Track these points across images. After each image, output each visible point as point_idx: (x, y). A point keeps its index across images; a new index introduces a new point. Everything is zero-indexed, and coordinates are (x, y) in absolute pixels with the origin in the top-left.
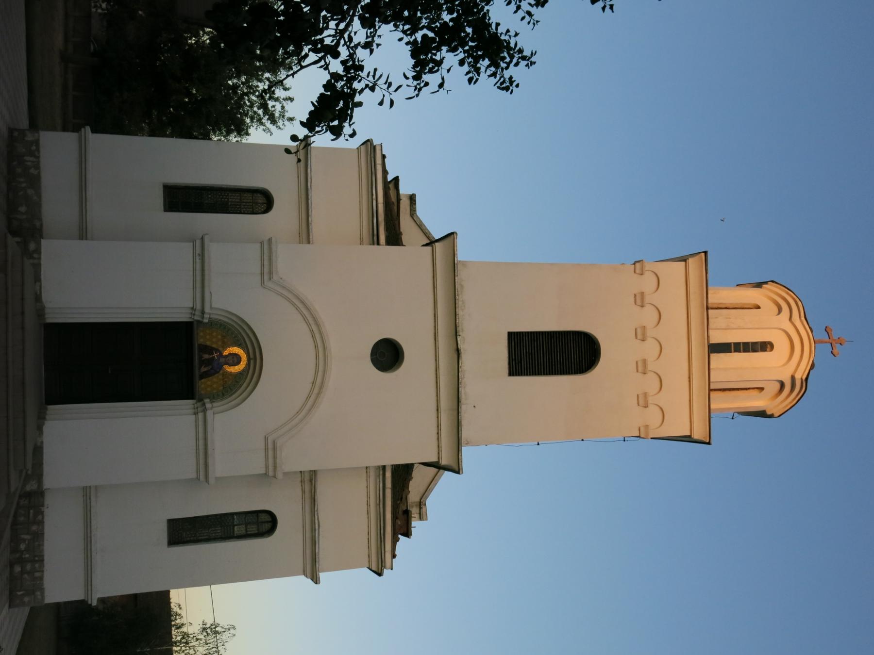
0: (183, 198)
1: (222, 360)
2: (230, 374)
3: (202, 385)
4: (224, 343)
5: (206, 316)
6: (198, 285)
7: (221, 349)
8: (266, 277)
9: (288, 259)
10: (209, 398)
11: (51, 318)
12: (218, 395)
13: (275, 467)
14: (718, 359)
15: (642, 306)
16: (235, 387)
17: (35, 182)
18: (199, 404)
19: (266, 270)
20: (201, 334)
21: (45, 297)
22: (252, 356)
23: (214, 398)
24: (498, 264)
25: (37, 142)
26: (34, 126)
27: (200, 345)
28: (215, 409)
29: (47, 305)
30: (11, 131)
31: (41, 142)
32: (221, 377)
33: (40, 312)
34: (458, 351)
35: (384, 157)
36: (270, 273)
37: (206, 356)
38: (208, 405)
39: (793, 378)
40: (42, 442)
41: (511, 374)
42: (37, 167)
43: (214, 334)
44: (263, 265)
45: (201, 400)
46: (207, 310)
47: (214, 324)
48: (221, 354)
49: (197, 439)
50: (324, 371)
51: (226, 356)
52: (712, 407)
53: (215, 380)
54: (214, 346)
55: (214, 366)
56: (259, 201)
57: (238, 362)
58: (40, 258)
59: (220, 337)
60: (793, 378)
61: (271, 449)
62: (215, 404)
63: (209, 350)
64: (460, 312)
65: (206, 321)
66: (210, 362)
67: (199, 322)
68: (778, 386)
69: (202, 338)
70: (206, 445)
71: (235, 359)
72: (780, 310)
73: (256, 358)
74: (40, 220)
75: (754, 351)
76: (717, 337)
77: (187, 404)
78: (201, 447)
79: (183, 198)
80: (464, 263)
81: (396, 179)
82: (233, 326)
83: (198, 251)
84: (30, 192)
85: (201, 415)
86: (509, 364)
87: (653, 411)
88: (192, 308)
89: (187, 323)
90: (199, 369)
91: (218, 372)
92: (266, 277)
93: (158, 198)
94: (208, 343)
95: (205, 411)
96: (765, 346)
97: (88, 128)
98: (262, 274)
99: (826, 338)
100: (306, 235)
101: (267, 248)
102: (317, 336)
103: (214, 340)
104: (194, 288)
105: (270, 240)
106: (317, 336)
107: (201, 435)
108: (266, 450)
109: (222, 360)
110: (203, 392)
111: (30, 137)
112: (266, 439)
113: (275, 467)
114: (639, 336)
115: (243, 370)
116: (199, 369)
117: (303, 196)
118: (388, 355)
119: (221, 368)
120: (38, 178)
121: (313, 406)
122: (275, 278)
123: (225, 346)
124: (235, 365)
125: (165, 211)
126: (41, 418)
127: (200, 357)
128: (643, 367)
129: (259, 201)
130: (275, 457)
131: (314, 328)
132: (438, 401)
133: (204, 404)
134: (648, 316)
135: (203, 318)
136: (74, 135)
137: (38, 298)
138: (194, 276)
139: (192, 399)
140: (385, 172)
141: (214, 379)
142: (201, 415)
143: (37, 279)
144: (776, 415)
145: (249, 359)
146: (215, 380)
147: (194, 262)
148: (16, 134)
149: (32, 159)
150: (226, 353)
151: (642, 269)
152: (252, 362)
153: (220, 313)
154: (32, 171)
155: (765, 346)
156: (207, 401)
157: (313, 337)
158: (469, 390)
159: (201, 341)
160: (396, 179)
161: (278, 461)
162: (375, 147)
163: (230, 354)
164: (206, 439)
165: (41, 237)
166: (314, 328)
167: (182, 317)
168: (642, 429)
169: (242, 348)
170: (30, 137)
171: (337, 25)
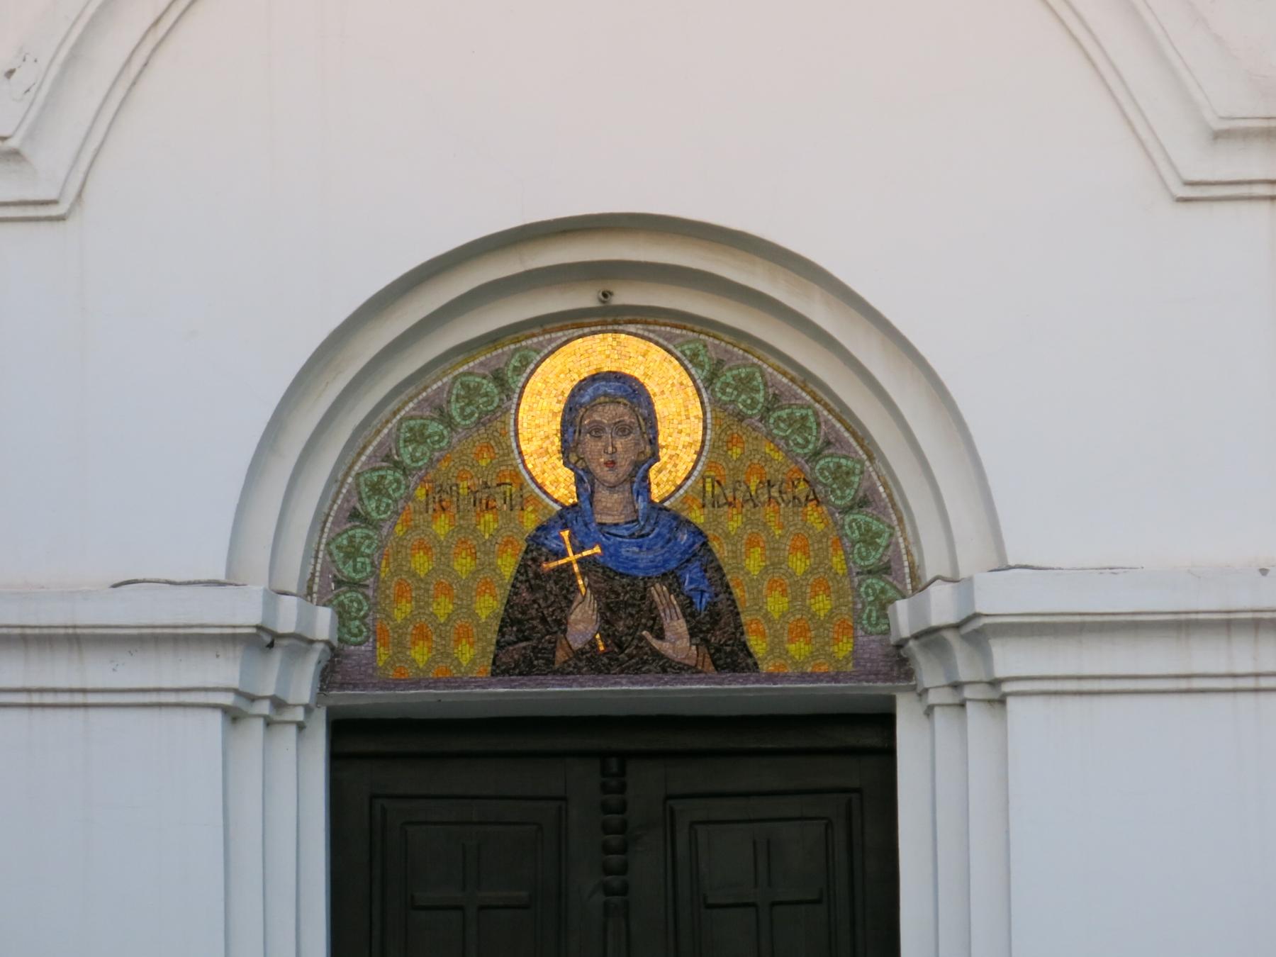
1: (612, 507)
2: (714, 448)
3: (793, 653)
4: (482, 501)
5: (288, 617)
6: (60, 671)
7: (530, 521)
10: (883, 606)
12: (377, 489)
18: (929, 673)
20: (420, 654)
22: (586, 298)
23: (888, 571)
27: (500, 669)
28: (970, 559)
32: (734, 523)
37: (583, 622)
38: (941, 606)
43: (421, 563)
46: (243, 610)
48: (567, 515)
49: (1187, 686)
51: (585, 479)
53: (754, 563)
54: (507, 566)
55: (656, 571)
57: (629, 391)
59: (441, 527)
62: (933, 564)
63: (528, 630)
65: (323, 623)
66: (626, 605)
69: (449, 656)
70: (1227, 625)
71: (606, 414)
77: (930, 762)
82: (354, 447)
85: (1009, 659)
88: (233, 716)
89: (337, 759)
90: (667, 666)
91: (701, 547)
94: (489, 607)
95: (976, 631)
103: (463, 565)
104: (80, 701)
109: (612, 507)
110: (844, 648)
112: (1197, 194)
115: (690, 361)
116: (667, 666)
119: (664, 518)
123: (511, 486)
124: (650, 423)
127: (589, 661)
133: (930, 636)
135: (302, 641)
139: (885, 721)
141: (747, 567)
142: (1009, 659)
145: (608, 318)
146: (754, 563)
150: (560, 484)
152: (626, 296)
156: (904, 618)
159: (471, 655)
163: (568, 450)
164: (1183, 626)
167: (293, 787)
169: (527, 366)
171: (414, 450)
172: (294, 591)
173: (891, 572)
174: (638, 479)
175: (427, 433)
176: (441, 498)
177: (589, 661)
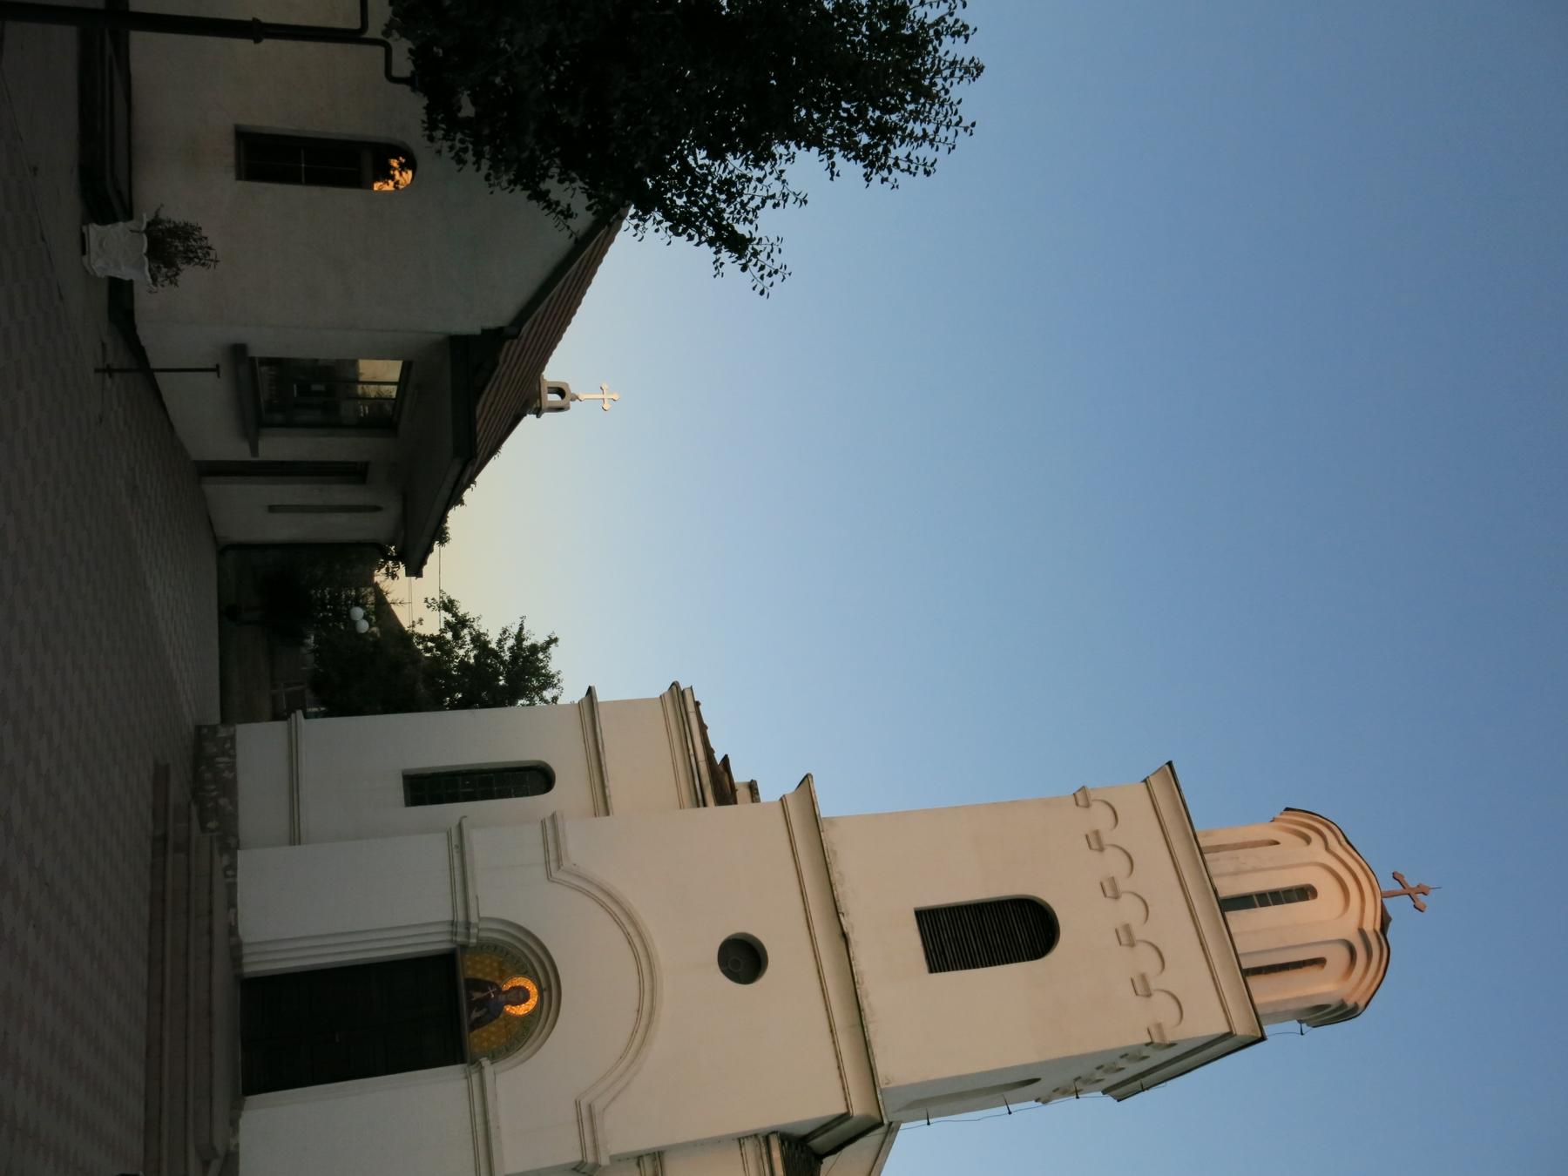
0: (427, 788)
1: (502, 998)
2: (517, 1018)
3: (475, 1039)
5: (474, 931)
6: (458, 887)
8: (553, 865)
9: (586, 843)
11: (256, 965)
13: (595, 1147)
14: (1240, 920)
15: (1149, 995)
16: (521, 1036)
17: (229, 788)
19: (552, 856)
21: (241, 931)
22: (544, 985)
24: (877, 816)
25: (232, 739)
26: (226, 719)
27: (467, 980)
29: (246, 939)
30: (199, 728)
31: (238, 738)
33: (236, 953)
34: (845, 936)
35: (697, 704)
36: (559, 859)
37: (477, 995)
39: (1362, 932)
40: (237, 1146)
41: (932, 969)
42: (232, 767)
44: (547, 851)
45: (475, 1062)
46: (474, 919)
47: (490, 948)
48: (499, 991)
50: (653, 989)
52: (1256, 1001)
55: (491, 1010)
56: (538, 778)
57: (526, 998)
58: (235, 876)
60: (1362, 932)
61: (587, 1119)
64: (839, 890)
67: (464, 947)
68: (1344, 953)
69: (470, 969)
70: (486, 1122)
72: (1308, 840)
73: (551, 989)
74: (236, 836)
75: (1289, 901)
76: (1228, 888)
77: (458, 1068)
78: (480, 1128)
79: (427, 788)
80: (831, 821)
81: (726, 759)
83: (455, 841)
84: (222, 801)
86: (927, 958)
87: (1161, 1001)
88: (453, 923)
90: (470, 1013)
91: (496, 1017)
92: (553, 865)
93: (398, 791)
94: (480, 976)
96: (1305, 893)
97: (300, 713)
98: (547, 863)
99: (1397, 887)
100: (603, 805)
101: (551, 829)
102: (636, 940)
104: (453, 893)
105: (553, 817)
106: (636, 940)
107: (478, 1109)
108: (579, 1121)
109: (502, 998)
111: (223, 733)
112: (577, 1104)
113: (595, 1147)
114: (1109, 893)
117: (594, 764)
118: (743, 958)
119: (501, 1010)
120: (234, 781)
121: (617, 902)
122: (566, 864)
123: (504, 975)
125: (407, 804)
126: (236, 1108)
127: (469, 997)
128: (1127, 937)
129: (538, 778)
130: (593, 1132)
131: (631, 929)
132: (838, 1055)
134: (1129, 910)
135: (468, 935)
136: (280, 726)
137: (233, 930)
138: (452, 877)
139: (463, 1061)
140: (709, 752)
141: (492, 1028)
142: (475, 1077)
143: (232, 904)
144: (1362, 1004)
147: (451, 858)
148: (205, 731)
149: (226, 759)
150: (506, 987)
151: (1087, 798)
152: (545, 994)
153: (495, 926)
154: (226, 774)
155: (1305, 893)
157: (630, 943)
158: (876, 997)
159: (470, 973)
160: (726, 759)
161: (599, 1135)
162: (683, 693)
163: (513, 988)
164: (485, 1113)
165: (237, 847)
166: (631, 929)
167: (435, 942)
168: (1153, 1031)
169: (530, 977)
170: (223, 733)
172: (554, 240)
173: (494, 1058)
174: (508, 1003)
175: (493, 645)
176: (501, 964)
177: (469, 997)
